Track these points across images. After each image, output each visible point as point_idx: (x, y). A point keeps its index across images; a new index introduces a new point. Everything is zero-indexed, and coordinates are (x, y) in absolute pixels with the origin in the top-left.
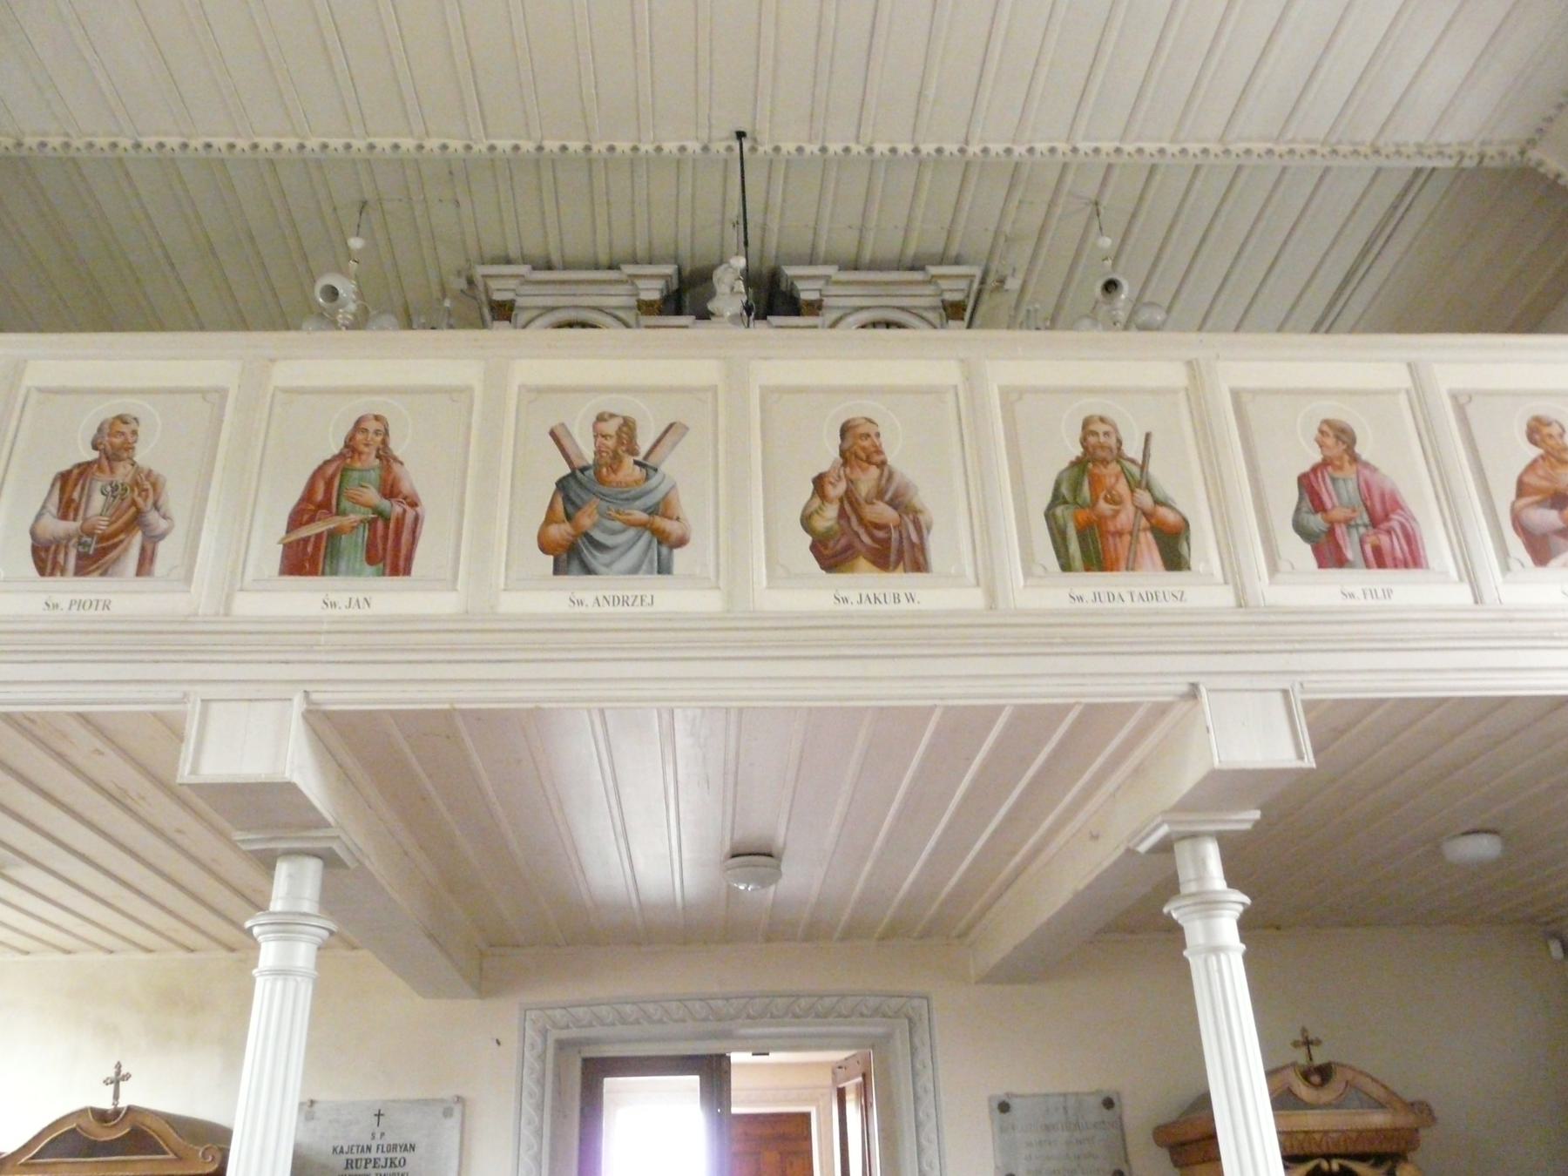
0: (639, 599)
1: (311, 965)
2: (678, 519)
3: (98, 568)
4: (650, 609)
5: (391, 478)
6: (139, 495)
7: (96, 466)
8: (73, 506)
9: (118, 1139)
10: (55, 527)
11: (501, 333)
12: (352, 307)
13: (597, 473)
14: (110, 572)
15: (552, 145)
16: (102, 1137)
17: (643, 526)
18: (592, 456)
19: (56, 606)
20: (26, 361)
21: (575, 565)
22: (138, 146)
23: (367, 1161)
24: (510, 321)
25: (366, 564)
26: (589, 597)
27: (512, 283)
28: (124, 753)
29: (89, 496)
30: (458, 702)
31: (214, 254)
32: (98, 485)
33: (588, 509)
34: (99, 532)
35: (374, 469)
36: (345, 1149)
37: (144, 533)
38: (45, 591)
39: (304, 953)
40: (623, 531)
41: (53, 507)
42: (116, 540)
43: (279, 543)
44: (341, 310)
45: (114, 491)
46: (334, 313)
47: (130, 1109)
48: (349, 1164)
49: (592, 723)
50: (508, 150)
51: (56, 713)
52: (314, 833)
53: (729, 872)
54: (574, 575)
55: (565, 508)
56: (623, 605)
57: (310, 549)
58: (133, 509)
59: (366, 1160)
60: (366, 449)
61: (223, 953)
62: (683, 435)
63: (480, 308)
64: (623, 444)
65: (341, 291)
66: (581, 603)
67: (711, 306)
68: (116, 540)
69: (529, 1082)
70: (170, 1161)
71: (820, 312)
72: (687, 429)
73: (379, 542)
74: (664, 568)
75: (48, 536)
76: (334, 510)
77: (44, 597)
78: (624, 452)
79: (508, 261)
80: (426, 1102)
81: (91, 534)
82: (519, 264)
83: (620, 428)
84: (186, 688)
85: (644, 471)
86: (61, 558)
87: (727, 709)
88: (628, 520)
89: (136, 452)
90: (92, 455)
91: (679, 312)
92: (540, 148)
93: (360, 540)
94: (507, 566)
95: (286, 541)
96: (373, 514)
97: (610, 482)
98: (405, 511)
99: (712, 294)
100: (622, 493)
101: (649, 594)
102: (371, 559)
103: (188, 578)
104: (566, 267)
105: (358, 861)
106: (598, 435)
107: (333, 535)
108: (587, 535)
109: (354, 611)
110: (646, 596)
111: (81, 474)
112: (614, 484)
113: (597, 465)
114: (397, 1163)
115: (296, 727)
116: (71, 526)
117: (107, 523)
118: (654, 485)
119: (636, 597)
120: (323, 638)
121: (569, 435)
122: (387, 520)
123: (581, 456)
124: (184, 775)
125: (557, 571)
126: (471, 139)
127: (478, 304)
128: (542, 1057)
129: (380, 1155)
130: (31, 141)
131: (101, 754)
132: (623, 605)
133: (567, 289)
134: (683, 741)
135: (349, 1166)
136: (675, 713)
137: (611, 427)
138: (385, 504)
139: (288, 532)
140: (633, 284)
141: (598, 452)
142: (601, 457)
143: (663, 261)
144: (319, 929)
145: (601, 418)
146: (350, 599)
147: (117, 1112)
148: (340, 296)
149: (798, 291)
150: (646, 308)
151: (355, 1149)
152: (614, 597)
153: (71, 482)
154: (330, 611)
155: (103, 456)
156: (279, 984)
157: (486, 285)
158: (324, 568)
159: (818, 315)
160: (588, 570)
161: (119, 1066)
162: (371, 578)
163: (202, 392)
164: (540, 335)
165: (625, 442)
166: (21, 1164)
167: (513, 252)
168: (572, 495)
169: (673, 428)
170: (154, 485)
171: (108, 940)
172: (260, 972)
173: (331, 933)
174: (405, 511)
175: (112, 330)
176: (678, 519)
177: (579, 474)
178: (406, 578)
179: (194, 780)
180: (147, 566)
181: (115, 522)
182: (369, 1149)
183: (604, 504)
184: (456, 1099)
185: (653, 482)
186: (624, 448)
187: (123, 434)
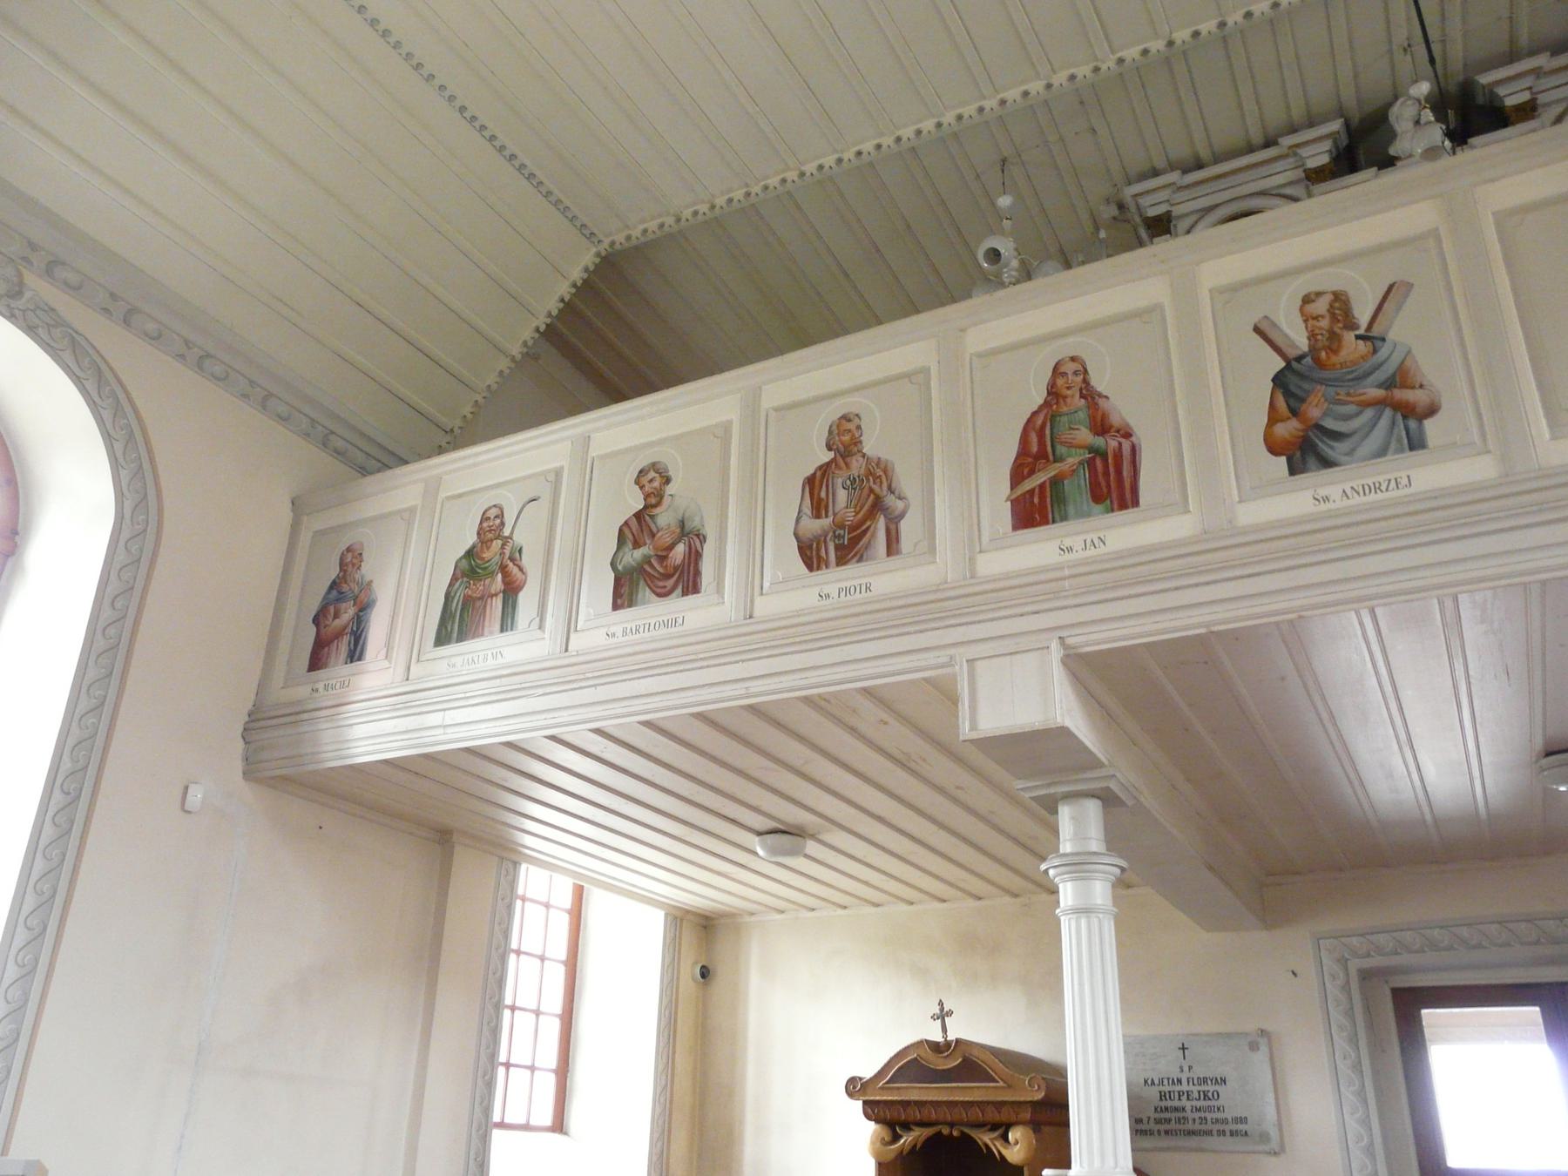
0: (1393, 483)
1: (1109, 902)
2: (1421, 386)
3: (855, 555)
4: (1407, 491)
5: (1100, 413)
6: (874, 483)
7: (834, 464)
8: (823, 504)
9: (955, 1066)
10: (813, 526)
11: (1163, 246)
12: (1015, 263)
13: (1317, 360)
14: (865, 557)
15: (1182, 35)
16: (938, 1066)
17: (1380, 403)
18: (1306, 342)
19: (828, 596)
20: (760, 388)
21: (1312, 461)
22: (802, 174)
23: (1180, 1094)
24: (1170, 234)
25: (1093, 504)
26: (1334, 492)
27: (1163, 195)
28: (905, 720)
29: (834, 495)
30: (1214, 625)
31: (878, 251)
32: (839, 481)
33: (1313, 399)
34: (849, 523)
35: (1081, 410)
36: (1156, 1082)
37: (885, 516)
38: (817, 585)
39: (1100, 891)
40: (1358, 414)
41: (807, 510)
42: (864, 527)
43: (1006, 501)
44: (1005, 270)
45: (853, 484)
46: (999, 275)
47: (958, 1041)
48: (1162, 1096)
49: (1361, 624)
50: (1041, 90)
51: (844, 691)
52: (1089, 775)
53: (1546, 773)
54: (1313, 471)
55: (1288, 404)
56: (1376, 492)
57: (1036, 500)
58: (872, 497)
59: (1179, 1092)
60: (1069, 392)
61: (1007, 899)
62: (1406, 296)
63: (1135, 230)
64: (1339, 321)
65: (1002, 251)
66: (1326, 499)
67: (1392, 151)
68: (864, 527)
69: (1337, 1016)
70: (1003, 1088)
71: (1536, 114)
72: (1412, 285)
73: (1101, 479)
74: (1416, 443)
75: (809, 535)
76: (1051, 458)
77: (816, 590)
78: (1341, 329)
79: (1155, 173)
80: (1229, 1035)
81: (842, 527)
82: (1168, 172)
83: (1331, 306)
84: (952, 651)
85: (1369, 343)
86: (823, 553)
87: (1525, 584)
88: (1362, 401)
89: (864, 444)
90: (827, 456)
91: (1353, 168)
92: (1171, 44)
93: (1082, 482)
94: (1237, 478)
95: (1014, 497)
96: (1089, 453)
97: (1334, 365)
98: (1120, 444)
99: (1392, 136)
100: (1349, 373)
101: (1404, 474)
102: (1097, 497)
103: (932, 549)
104: (1217, 160)
105: (1135, 798)
106: (1307, 318)
107: (1056, 482)
108: (1319, 428)
109: (1091, 552)
110: (1401, 478)
111: (823, 475)
112: (1339, 366)
113: (1313, 350)
114: (1210, 1095)
115: (1058, 673)
116: (826, 522)
117: (853, 514)
118: (1383, 358)
119: (1390, 481)
120: (1067, 583)
121: (1274, 325)
122: (1104, 456)
123: (1294, 345)
124: (966, 731)
125: (1293, 471)
126: (1097, 60)
127: (1133, 226)
128: (1346, 988)
129: (1191, 1087)
130: (720, 201)
131: (886, 723)
132: (1376, 492)
133: (1222, 184)
134: (1472, 631)
135: (1163, 1098)
136: (1460, 600)
137: (1321, 306)
138: (1099, 441)
139: (1012, 489)
140: (1295, 154)
141: (1312, 336)
142: (1316, 340)
143: (1325, 119)
144: (1110, 866)
145: (1307, 300)
146: (1085, 541)
147: (948, 1044)
148: (1003, 256)
149: (1501, 99)
150: (1317, 176)
151: (1166, 1082)
152: (1363, 486)
153: (817, 483)
154: (1068, 557)
155: (838, 454)
156: (1083, 922)
157: (1137, 205)
158: (1053, 518)
159: (1533, 118)
160: (1327, 463)
161: (941, 1004)
162: (1101, 516)
163: (907, 376)
164: (1207, 235)
165: (1340, 318)
166: (880, 1088)
167: (1160, 163)
168: (1293, 389)
169: (1395, 288)
170: (885, 471)
171: (811, 902)
172: (1062, 912)
173: (1123, 869)
174: (1120, 444)
175: (682, 383)
176: (1421, 386)
177: (1295, 365)
178: (1135, 509)
179: (974, 735)
180: (894, 545)
181: (861, 509)
182: (1179, 1081)
183: (1331, 390)
184: (1260, 1032)
185: (1384, 352)
186: (1341, 325)
187: (850, 431)
